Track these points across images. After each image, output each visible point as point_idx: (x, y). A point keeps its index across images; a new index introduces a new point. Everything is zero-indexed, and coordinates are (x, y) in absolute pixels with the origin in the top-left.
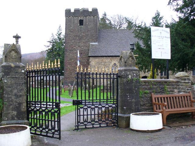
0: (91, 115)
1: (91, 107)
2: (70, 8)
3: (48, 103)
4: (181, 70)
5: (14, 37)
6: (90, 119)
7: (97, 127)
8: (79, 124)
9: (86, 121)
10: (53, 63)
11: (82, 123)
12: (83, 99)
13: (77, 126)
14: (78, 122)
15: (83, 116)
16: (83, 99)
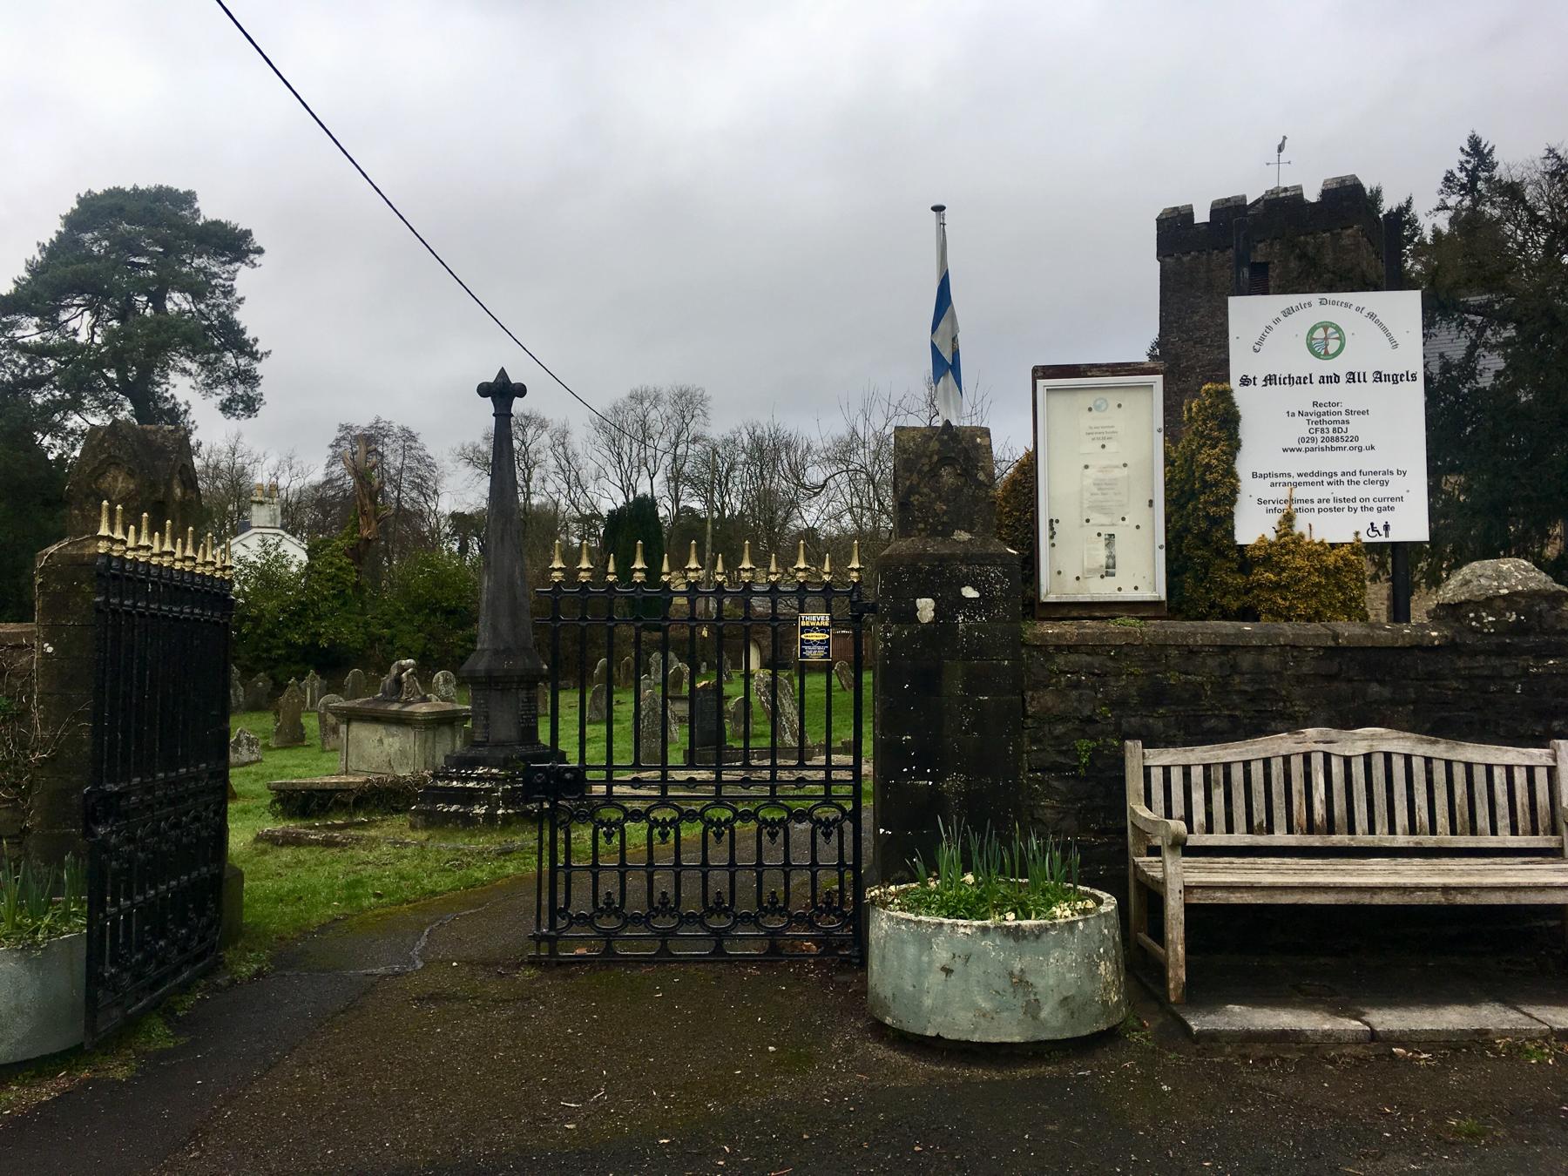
0: (595, 868)
1: (761, 813)
2: (1180, 202)
3: (768, 777)
4: (1502, 553)
5: (484, 390)
6: (752, 896)
7: (638, 962)
8: (561, 923)
9: (718, 909)
10: (160, 536)
11: (587, 920)
12: (595, 753)
13: (544, 937)
14: (554, 912)
15: (780, 875)
16: (595, 753)
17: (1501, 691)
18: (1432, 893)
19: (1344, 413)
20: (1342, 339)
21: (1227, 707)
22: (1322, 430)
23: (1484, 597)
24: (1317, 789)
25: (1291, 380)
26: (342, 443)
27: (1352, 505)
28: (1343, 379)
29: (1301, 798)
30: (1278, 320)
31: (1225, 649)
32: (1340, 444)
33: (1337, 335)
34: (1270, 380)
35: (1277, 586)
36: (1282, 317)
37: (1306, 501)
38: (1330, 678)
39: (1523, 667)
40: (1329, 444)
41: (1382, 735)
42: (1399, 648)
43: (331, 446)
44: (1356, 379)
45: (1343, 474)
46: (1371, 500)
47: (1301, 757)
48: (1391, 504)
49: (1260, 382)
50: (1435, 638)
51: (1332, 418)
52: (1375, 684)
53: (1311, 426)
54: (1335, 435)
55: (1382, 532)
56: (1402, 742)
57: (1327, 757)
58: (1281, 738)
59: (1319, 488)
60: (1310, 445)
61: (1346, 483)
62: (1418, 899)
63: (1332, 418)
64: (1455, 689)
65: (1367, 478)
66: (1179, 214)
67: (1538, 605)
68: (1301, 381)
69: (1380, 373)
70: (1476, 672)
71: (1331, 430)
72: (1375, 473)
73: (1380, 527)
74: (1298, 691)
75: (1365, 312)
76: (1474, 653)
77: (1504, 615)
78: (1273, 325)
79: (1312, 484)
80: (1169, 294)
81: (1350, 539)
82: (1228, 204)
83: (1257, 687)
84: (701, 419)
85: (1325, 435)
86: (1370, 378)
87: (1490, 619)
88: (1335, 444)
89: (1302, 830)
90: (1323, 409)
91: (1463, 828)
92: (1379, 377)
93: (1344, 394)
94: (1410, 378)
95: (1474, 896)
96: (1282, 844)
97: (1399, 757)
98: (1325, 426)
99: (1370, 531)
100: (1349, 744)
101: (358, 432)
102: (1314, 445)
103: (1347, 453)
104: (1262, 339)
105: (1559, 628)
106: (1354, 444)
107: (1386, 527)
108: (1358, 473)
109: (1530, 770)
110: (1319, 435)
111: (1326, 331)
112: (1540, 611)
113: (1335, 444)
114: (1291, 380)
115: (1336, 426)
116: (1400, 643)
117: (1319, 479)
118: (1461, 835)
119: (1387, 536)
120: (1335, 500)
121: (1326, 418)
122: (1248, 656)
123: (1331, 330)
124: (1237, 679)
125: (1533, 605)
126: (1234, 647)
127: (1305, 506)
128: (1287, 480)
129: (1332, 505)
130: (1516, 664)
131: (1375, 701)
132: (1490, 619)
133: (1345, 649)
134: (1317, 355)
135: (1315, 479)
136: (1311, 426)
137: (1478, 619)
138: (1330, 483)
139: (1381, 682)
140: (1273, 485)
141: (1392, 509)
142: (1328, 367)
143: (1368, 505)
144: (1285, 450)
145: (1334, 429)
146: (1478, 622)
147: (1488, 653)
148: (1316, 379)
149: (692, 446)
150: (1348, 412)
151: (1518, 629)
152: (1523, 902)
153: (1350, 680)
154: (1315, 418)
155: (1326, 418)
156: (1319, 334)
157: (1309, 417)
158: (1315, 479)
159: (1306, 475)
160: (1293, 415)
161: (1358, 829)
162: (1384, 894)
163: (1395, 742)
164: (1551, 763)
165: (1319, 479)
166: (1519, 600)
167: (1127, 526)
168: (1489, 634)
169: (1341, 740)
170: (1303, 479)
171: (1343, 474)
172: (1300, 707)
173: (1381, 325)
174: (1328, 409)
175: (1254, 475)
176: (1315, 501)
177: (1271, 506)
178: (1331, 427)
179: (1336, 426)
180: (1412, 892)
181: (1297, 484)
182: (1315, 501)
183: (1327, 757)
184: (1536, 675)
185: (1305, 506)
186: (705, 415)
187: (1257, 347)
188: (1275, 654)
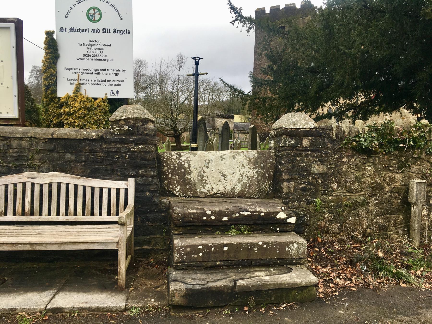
2: (261, 6)
17: (119, 158)
18: (25, 246)
19: (101, 45)
20: (100, 14)
21: (5, 162)
22: (93, 52)
23: (114, 120)
24: (27, 197)
25: (80, 30)
26: (33, 71)
27: (104, 83)
28: (101, 31)
29: (20, 201)
30: (75, 5)
31: (6, 138)
32: (100, 58)
33: (99, 13)
34: (72, 30)
35: (69, 114)
36: (76, 4)
37: (86, 80)
38: (51, 151)
39: (129, 148)
40: (95, 58)
41: (56, 175)
42: (79, 139)
43: (30, 72)
44: (106, 32)
45: (101, 70)
46: (112, 81)
47: (21, 184)
48: (119, 83)
49: (68, 30)
50: (94, 136)
51: (97, 47)
52: (69, 154)
53: (88, 50)
54: (98, 54)
55: (116, 94)
56: (65, 178)
57: (33, 185)
58: (14, 176)
59: (105, 75)
60: (88, 58)
61: (102, 74)
62: (19, 248)
63: (97, 47)
64: (101, 157)
65: (110, 72)
66: (261, 10)
67: (138, 123)
68: (85, 31)
69: (116, 29)
70: (110, 150)
71: (96, 52)
72: (113, 70)
73: (115, 92)
74: (36, 156)
75: (110, 4)
76: (110, 142)
77: (123, 127)
78: (73, 7)
79: (89, 73)
80: (258, 34)
81: (103, 96)
82: (275, 8)
83: (19, 154)
84: (145, 69)
85: (94, 54)
86: (112, 31)
87: (117, 128)
88: (98, 58)
89: (19, 214)
90: (93, 43)
91: (88, 213)
92: (115, 31)
93: (101, 37)
94: (127, 32)
95: (45, 247)
96: (9, 220)
97: (64, 184)
98: (94, 50)
99: (111, 93)
100: (42, 179)
101: (38, 68)
102: (89, 58)
103: (103, 61)
104: (69, 12)
105: (145, 133)
106: (105, 58)
107: (118, 92)
108: (107, 70)
109: (118, 190)
110: (91, 54)
111: (94, 11)
112: (138, 126)
113: (98, 58)
114: (80, 30)
115: (98, 50)
116: (79, 137)
117: (91, 72)
118: (87, 216)
119: (118, 96)
120: (98, 80)
121: (94, 47)
122: (16, 141)
123: (96, 10)
124: (11, 151)
125: (136, 123)
126: (9, 138)
127: (86, 82)
128: (78, 71)
129: (96, 82)
130: (126, 147)
131: (69, 161)
132: (117, 128)
133: (57, 139)
134: (91, 20)
135: (90, 72)
136: (88, 50)
137: (113, 128)
138: (95, 74)
139: (71, 153)
140: (73, 73)
141: (120, 85)
142: (95, 26)
143: (111, 83)
144: (78, 59)
145: (97, 52)
146: (113, 130)
147: (116, 142)
148: (90, 30)
149: (142, 77)
150: (103, 45)
151: (128, 133)
152: (66, 249)
153: (58, 152)
154: (89, 47)
155: (94, 47)
156: (92, 12)
157: (87, 46)
158: (90, 72)
159: (86, 70)
160: (81, 45)
161: (43, 214)
162: (4, 246)
163: (62, 178)
164: (126, 187)
165: (91, 72)
166: (131, 121)
167: (3, 87)
168: (117, 134)
169: (39, 177)
170: (85, 71)
171: (101, 70)
172: (37, 163)
173: (116, 9)
174: (95, 43)
175: (65, 69)
176: (90, 80)
177: (72, 82)
178: (96, 51)
179: (98, 50)
180: (17, 245)
181: (82, 74)
182: (90, 80)
183: (33, 185)
184: (134, 151)
185: (86, 82)
186: (146, 68)
187: (67, 16)
188: (27, 141)
